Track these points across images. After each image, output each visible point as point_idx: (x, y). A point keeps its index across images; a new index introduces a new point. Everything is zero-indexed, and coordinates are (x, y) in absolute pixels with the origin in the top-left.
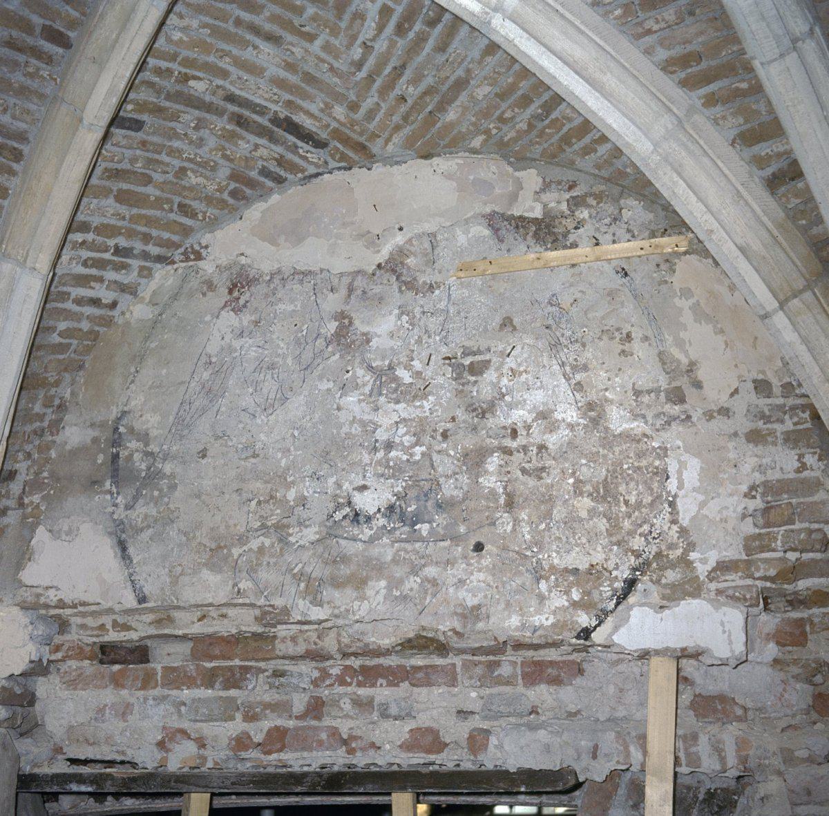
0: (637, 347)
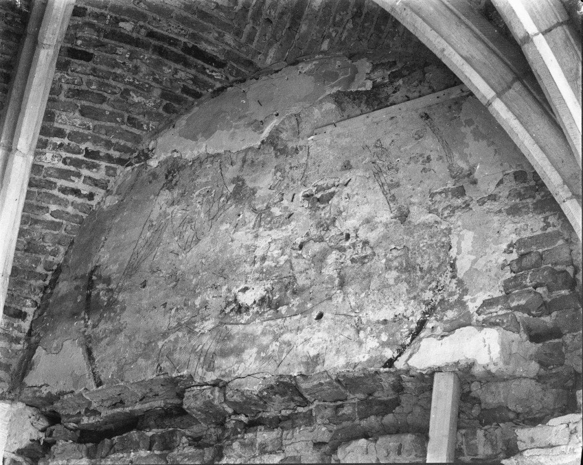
0: (435, 165)
